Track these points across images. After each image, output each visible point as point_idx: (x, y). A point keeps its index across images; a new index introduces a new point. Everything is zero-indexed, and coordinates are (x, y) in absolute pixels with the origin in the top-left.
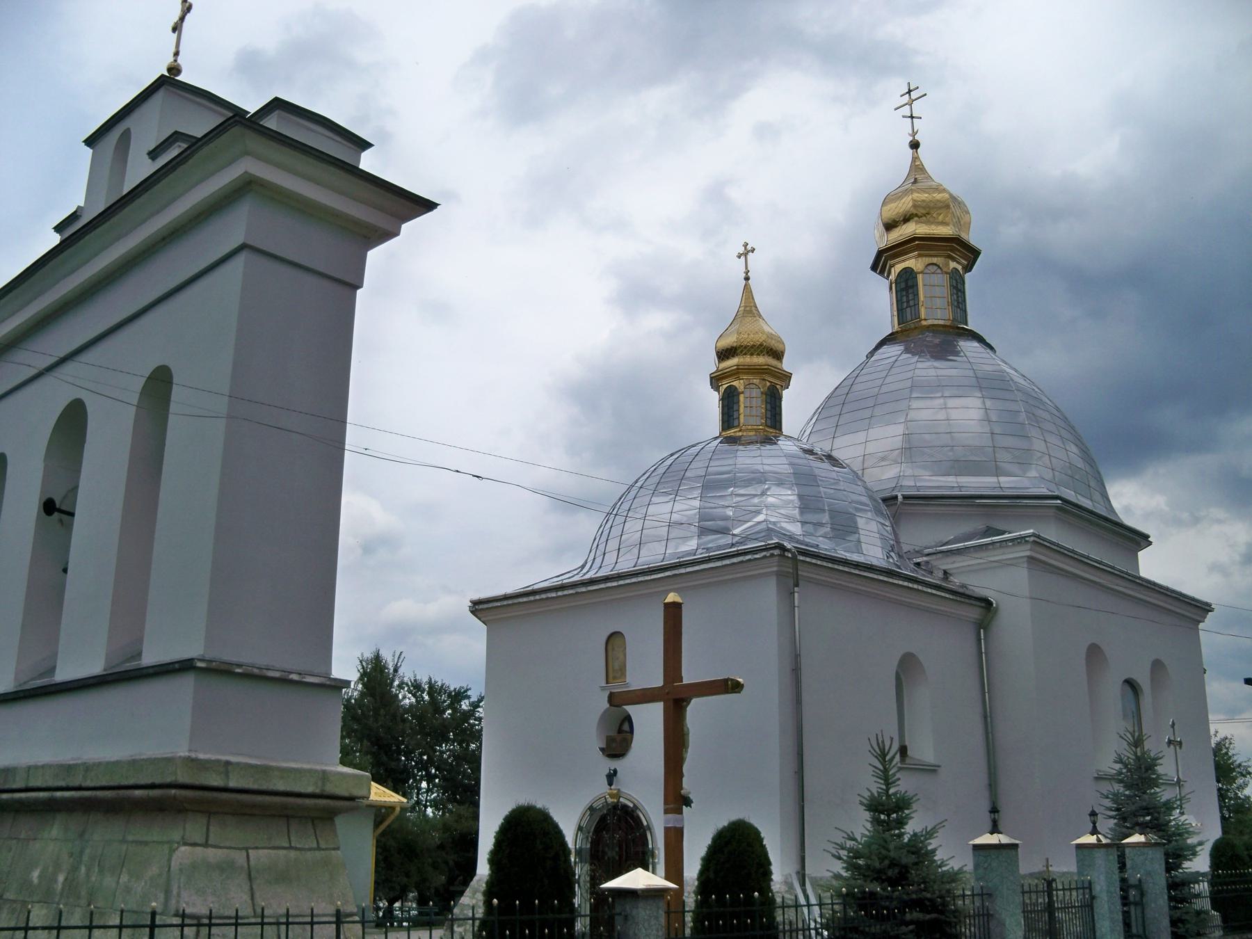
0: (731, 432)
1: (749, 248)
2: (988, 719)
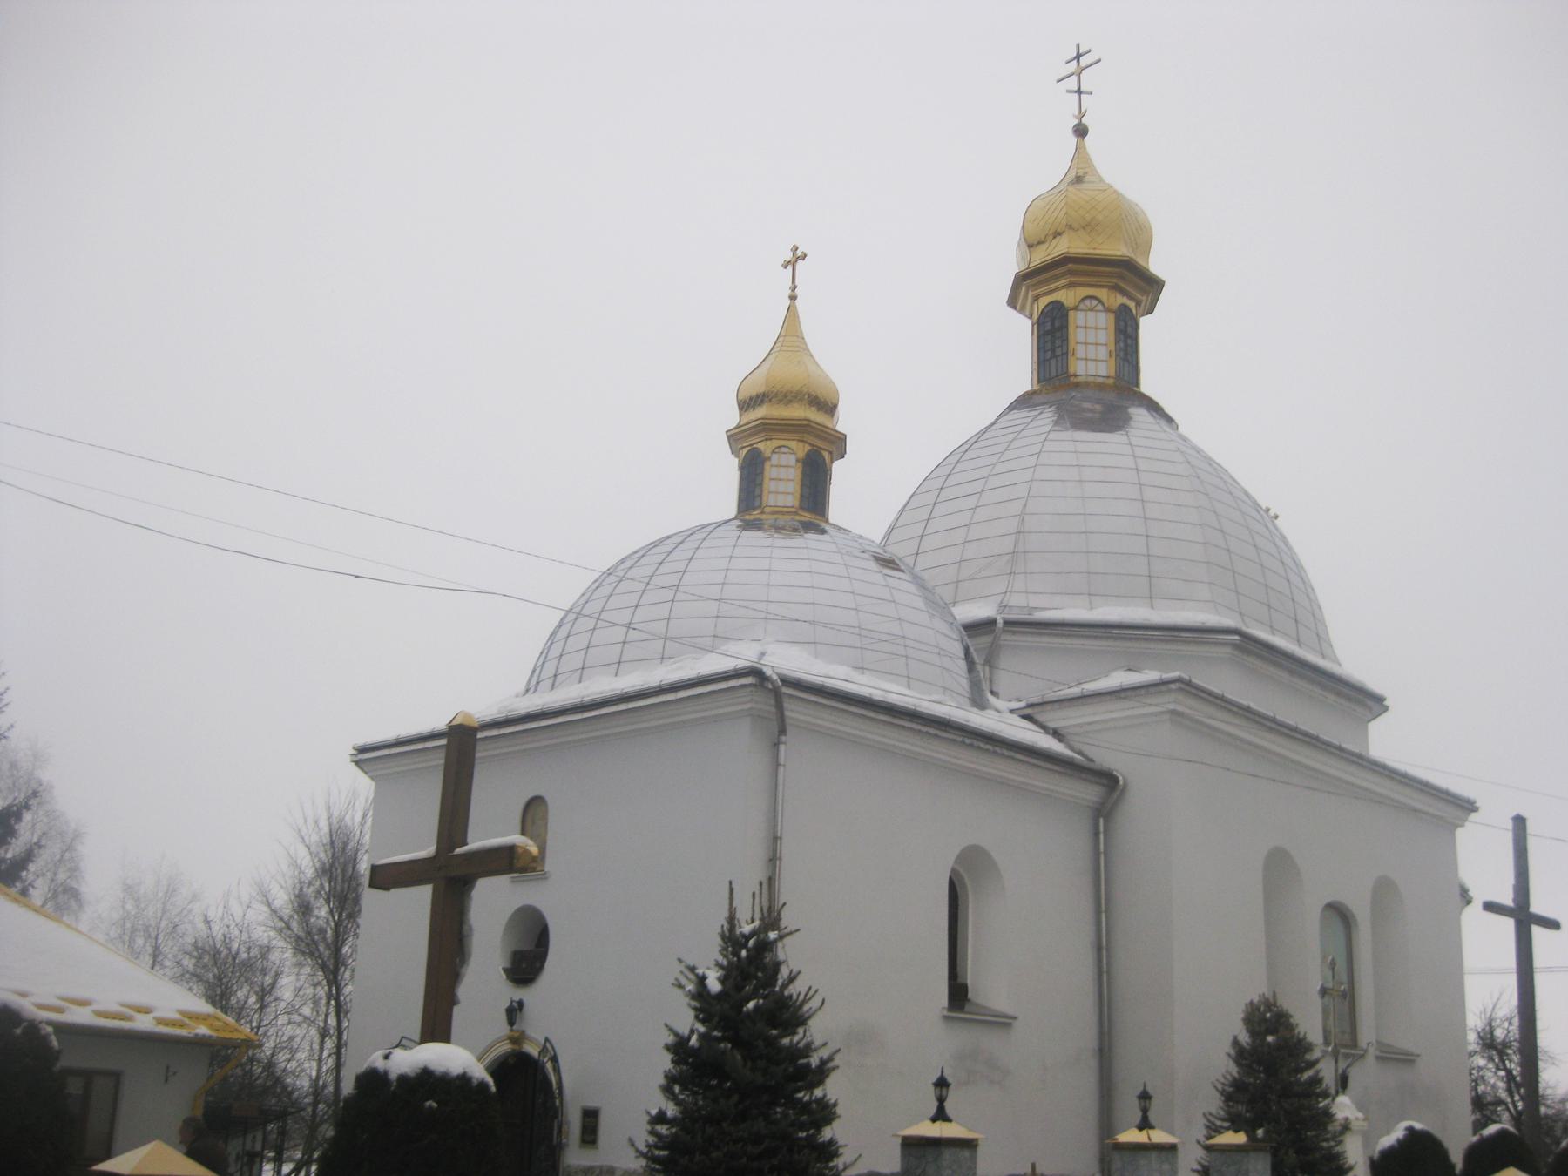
0: (755, 514)
1: (799, 253)
2: (1103, 949)
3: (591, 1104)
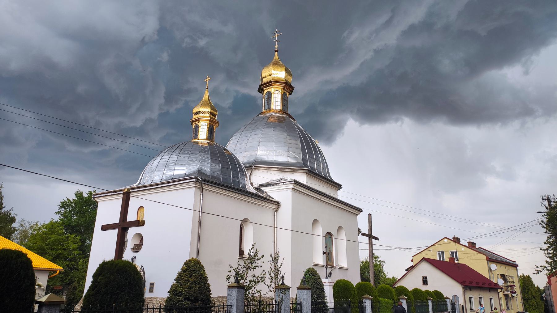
3: (152, 282)
